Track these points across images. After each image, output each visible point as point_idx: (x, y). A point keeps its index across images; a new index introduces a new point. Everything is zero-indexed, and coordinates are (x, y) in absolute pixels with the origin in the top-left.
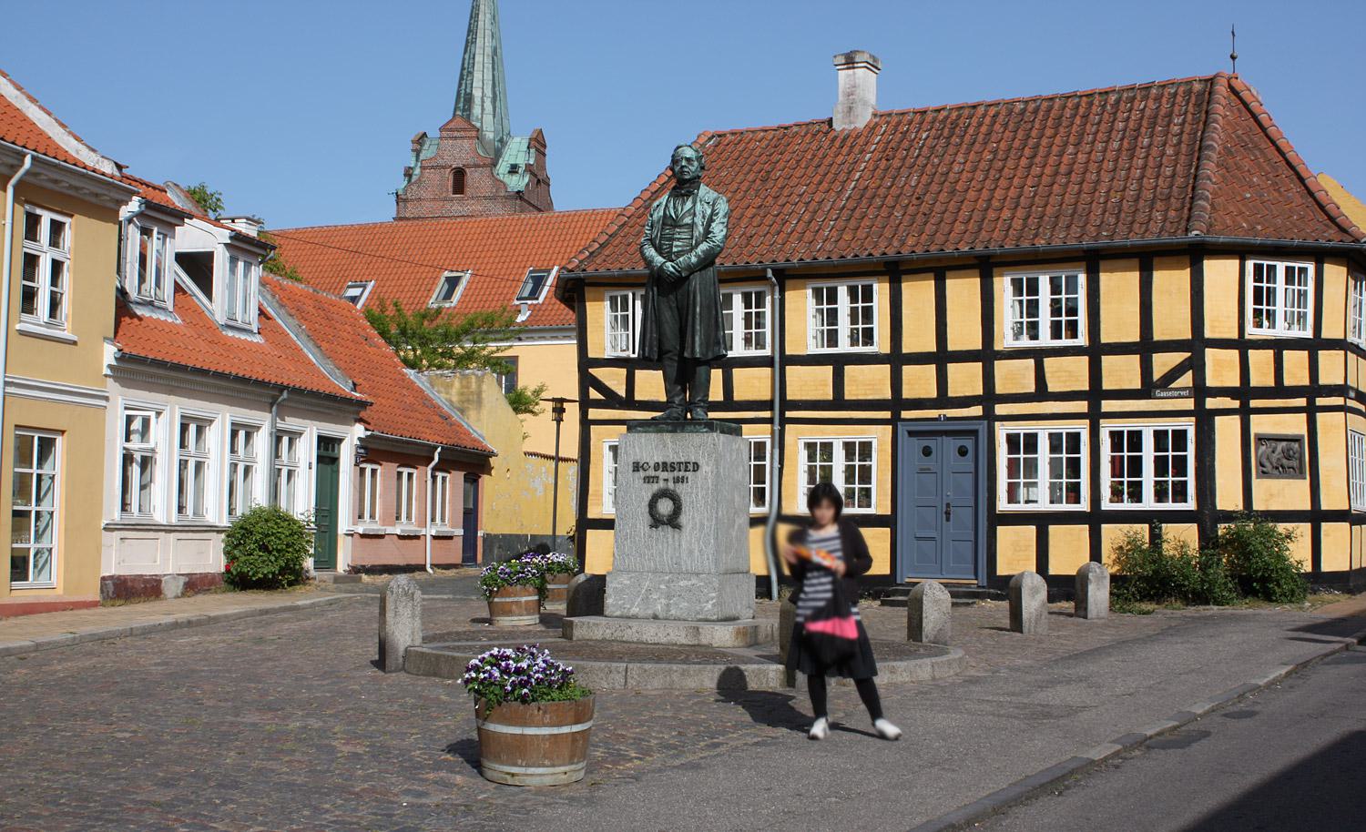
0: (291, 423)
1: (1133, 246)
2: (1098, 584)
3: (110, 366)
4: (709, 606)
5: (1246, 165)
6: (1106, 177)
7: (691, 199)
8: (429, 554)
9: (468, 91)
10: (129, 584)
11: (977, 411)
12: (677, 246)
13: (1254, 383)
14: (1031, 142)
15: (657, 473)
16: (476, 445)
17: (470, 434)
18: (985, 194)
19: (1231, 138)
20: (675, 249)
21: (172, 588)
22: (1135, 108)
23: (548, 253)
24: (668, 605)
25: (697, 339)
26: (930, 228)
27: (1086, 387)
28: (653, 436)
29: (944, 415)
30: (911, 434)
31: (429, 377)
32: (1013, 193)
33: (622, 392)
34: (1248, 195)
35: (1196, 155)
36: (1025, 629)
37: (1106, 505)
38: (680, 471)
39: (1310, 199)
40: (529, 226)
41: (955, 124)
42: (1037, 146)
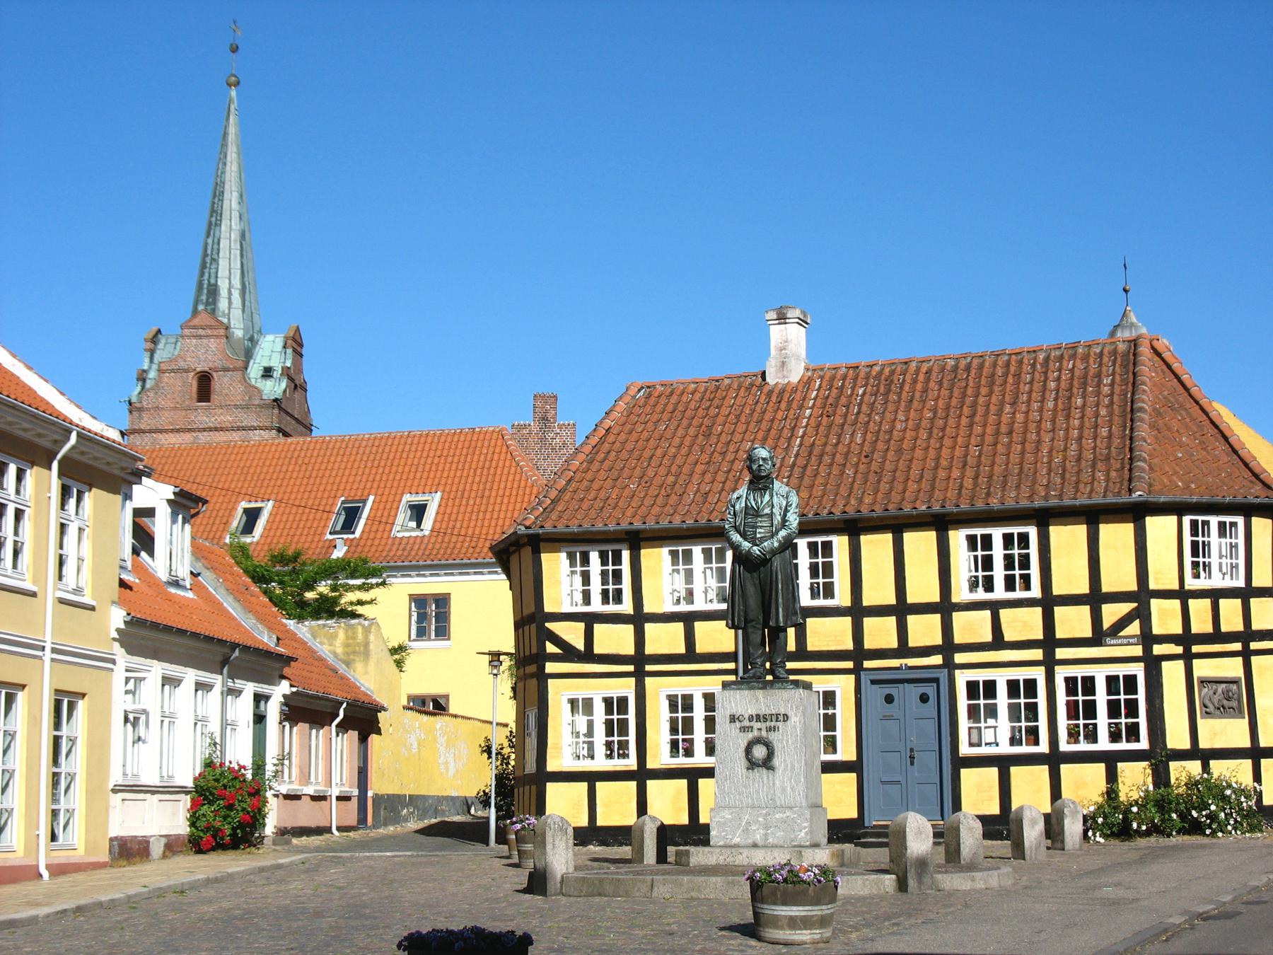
0: (239, 683)
1: (1082, 506)
2: (1073, 819)
3: (118, 630)
4: (803, 834)
5: (1175, 425)
6: (1046, 438)
7: (768, 492)
8: (335, 815)
9: (213, 281)
10: (129, 845)
11: (937, 660)
12: (760, 533)
13: (1195, 630)
14: (969, 400)
15: (752, 724)
16: (363, 698)
17: (359, 688)
18: (932, 454)
19: (1159, 399)
20: (758, 536)
21: (157, 849)
22: (1064, 367)
23: (323, 476)
24: (766, 835)
25: (781, 610)
26: (884, 487)
27: (1040, 636)
28: (746, 692)
29: (906, 665)
30: (873, 682)
31: (311, 628)
32: (959, 452)
33: (580, 645)
34: (1180, 455)
35: (1129, 416)
36: (1027, 857)
37: (1064, 746)
38: (772, 721)
39: (1235, 457)
40: (336, 450)
41: (889, 381)
42: (974, 405)
